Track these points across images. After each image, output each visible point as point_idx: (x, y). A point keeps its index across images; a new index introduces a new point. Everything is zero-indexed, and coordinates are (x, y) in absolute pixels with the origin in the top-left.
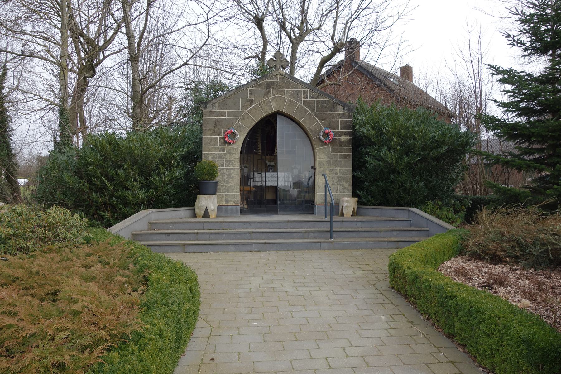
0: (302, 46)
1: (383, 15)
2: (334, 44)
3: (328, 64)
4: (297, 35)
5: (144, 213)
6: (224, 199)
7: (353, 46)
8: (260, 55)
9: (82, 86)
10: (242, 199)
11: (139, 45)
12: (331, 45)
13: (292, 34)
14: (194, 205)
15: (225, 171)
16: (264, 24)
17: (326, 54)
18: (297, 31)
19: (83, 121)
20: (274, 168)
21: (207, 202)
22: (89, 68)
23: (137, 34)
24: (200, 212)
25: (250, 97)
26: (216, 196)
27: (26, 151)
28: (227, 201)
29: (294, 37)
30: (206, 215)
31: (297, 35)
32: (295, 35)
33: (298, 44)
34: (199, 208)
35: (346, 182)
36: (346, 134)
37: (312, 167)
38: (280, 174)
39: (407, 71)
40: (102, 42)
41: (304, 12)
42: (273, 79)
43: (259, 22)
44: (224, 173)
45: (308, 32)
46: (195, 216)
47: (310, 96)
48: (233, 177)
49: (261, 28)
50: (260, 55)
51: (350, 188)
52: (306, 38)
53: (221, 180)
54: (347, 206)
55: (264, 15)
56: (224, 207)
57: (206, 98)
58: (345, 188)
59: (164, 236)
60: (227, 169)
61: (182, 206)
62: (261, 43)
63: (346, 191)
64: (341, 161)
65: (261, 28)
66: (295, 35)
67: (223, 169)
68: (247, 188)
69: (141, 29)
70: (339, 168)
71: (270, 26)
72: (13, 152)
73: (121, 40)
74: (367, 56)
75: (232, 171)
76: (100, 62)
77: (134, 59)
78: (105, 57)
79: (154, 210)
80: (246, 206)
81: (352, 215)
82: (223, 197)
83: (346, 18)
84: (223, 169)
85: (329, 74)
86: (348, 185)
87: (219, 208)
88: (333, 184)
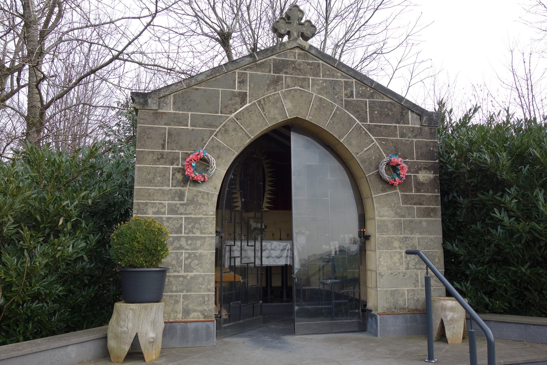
6: (180, 307)
15: (183, 242)
28: (186, 312)
30: (135, 352)
36: (427, 168)
44: (181, 247)
60: (187, 238)
67: (178, 239)
70: (417, 236)
82: (177, 302)
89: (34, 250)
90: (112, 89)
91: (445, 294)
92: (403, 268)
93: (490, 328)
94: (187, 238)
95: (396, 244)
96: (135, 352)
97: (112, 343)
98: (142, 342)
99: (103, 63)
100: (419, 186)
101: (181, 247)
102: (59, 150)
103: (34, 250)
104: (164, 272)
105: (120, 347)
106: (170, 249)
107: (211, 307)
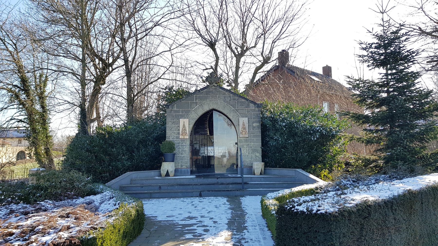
0: (242, 59)
1: (297, 37)
2: (263, 58)
3: (261, 70)
4: (240, 52)
5: (128, 173)
6: (180, 165)
7: (284, 56)
8: (214, 67)
9: (96, 91)
10: (192, 165)
11: (131, 66)
12: (261, 58)
13: (236, 51)
14: (160, 169)
15: (180, 147)
16: (216, 47)
17: (259, 64)
18: (239, 49)
19: (98, 114)
20: (212, 144)
21: (167, 167)
22: (100, 80)
23: (130, 59)
24: (163, 173)
26: (174, 163)
27: (59, 135)
28: (182, 166)
29: (237, 54)
30: (167, 174)
31: (240, 52)
32: (238, 52)
34: (163, 170)
36: (256, 122)
37: (236, 144)
38: (216, 148)
39: (327, 70)
40: (111, 60)
41: (244, 35)
42: (209, 89)
43: (212, 45)
44: (180, 148)
45: (248, 49)
46: (160, 175)
49: (214, 50)
50: (214, 67)
51: (260, 157)
52: (245, 54)
54: (257, 168)
55: (216, 41)
56: (179, 170)
57: (175, 98)
59: (139, 188)
60: (181, 146)
62: (213, 59)
65: (214, 50)
66: (238, 52)
67: (179, 146)
68: (195, 157)
69: (133, 55)
70: (253, 144)
71: (220, 46)
72: (50, 134)
73: (120, 62)
74: (297, 61)
76: (110, 73)
77: (129, 73)
78: (113, 70)
79: (134, 172)
80: (194, 169)
81: (261, 174)
82: (179, 163)
83: (272, 39)
84: (179, 146)
85: (263, 79)
86: (259, 155)
87: (176, 171)
89: (222, 78)
90: (92, 63)
91: (261, 160)
92: (247, 154)
93: (302, 184)
94: (181, 146)
95: (245, 146)
96: (167, 174)
97: (162, 172)
98: (169, 172)
99: (190, 129)
100: (254, 127)
101: (180, 148)
102: (36, 150)
103: (222, 78)
104: (174, 154)
105: (163, 173)
106: (177, 149)
107: (189, 164)
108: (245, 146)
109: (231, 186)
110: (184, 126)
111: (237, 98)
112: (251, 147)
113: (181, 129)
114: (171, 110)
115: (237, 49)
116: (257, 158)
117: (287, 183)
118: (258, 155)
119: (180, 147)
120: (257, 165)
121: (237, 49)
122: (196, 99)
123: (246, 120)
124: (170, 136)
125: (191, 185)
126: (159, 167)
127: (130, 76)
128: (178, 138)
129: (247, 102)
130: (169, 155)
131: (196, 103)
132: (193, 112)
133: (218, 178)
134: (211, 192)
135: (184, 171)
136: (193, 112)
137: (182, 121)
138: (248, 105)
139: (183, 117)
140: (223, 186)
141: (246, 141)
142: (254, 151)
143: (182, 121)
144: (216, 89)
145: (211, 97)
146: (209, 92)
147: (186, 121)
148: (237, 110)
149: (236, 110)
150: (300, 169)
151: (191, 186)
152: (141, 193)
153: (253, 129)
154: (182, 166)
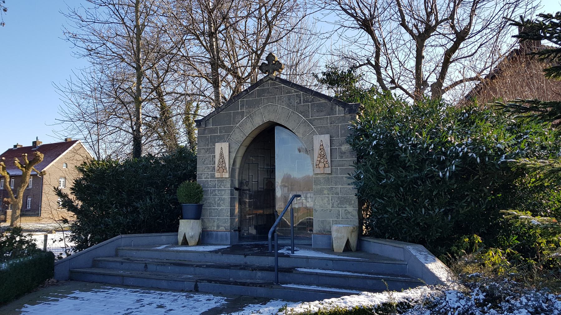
6: (215, 224)
15: (217, 192)
17: (449, 46)
25: (241, 109)
28: (218, 227)
33: (423, 41)
35: (350, 205)
43: (367, 25)
44: (216, 195)
47: (304, 100)
48: (224, 199)
49: (371, 33)
53: (213, 202)
54: (337, 238)
56: (214, 233)
58: (349, 212)
59: (118, 264)
60: (219, 190)
61: (164, 232)
63: (349, 216)
64: (342, 177)
67: (215, 190)
75: (223, 192)
84: (215, 190)
88: (333, 207)
92: (330, 207)
100: (342, 154)
101: (216, 195)
104: (202, 205)
108: (326, 192)
109: (259, 274)
110: (221, 155)
111: (311, 97)
112: (337, 193)
113: (219, 163)
114: (205, 130)
115: (416, 26)
116: (349, 216)
117: (375, 279)
118: (350, 209)
119: (217, 192)
120: (337, 231)
121: (416, 26)
122: (242, 106)
123: (326, 139)
124: (203, 174)
125: (192, 265)
126: (175, 229)
127: (218, 86)
128: (213, 176)
129: (329, 104)
130: (189, 207)
131: (242, 114)
132: (237, 131)
133: (245, 256)
134: (213, 284)
135: (222, 235)
136: (237, 131)
137: (218, 146)
138: (332, 109)
139: (221, 139)
140: (246, 273)
141: (328, 181)
142: (343, 201)
143: (218, 146)
144: (274, 84)
145: (266, 101)
146: (263, 91)
147: (225, 146)
148: (311, 121)
149: (310, 121)
150: (421, 247)
151: (192, 269)
152: (110, 275)
153: (342, 157)
154: (218, 227)
